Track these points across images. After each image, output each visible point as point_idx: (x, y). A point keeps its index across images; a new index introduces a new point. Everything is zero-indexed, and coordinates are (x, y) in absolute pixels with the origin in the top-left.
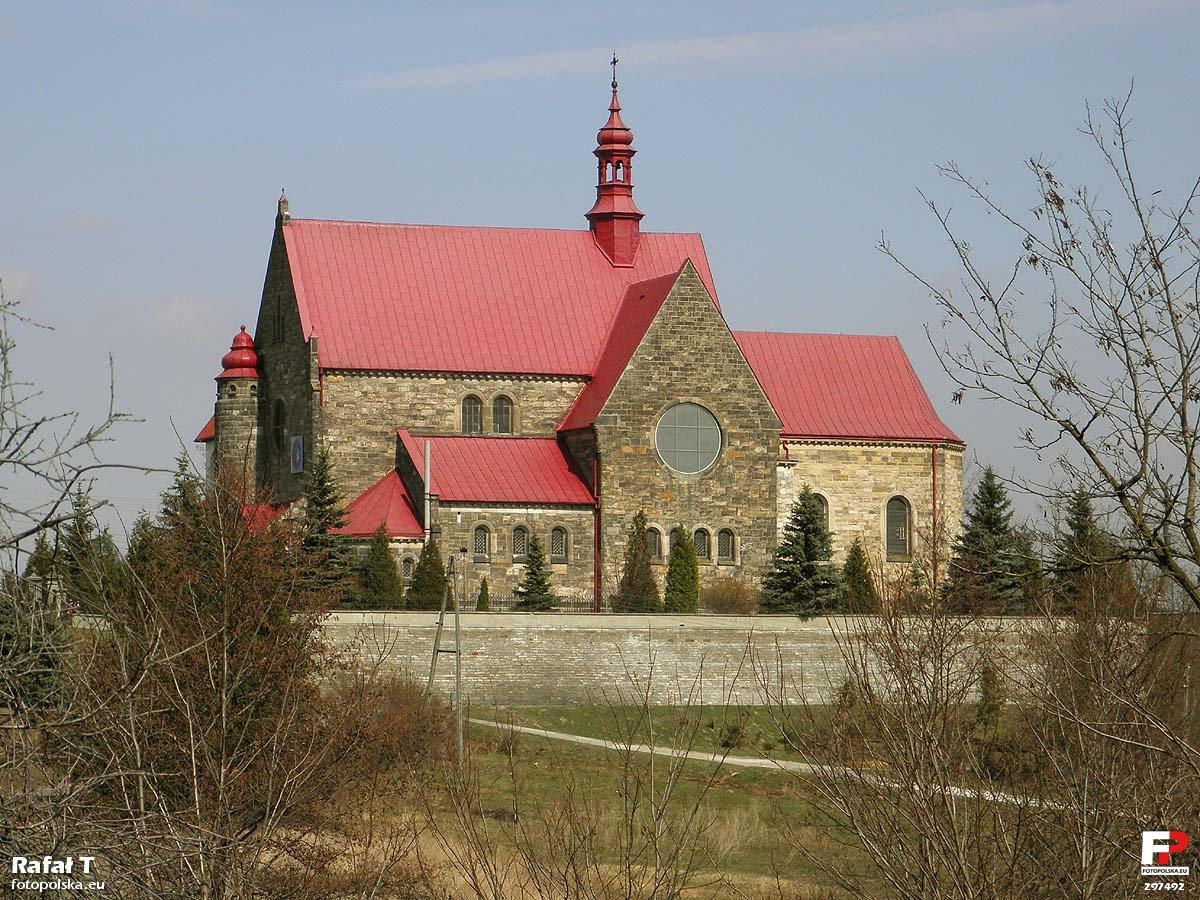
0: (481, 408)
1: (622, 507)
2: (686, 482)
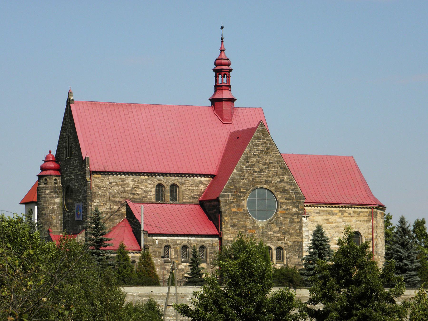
0: (164, 190)
1: (232, 236)
2: (261, 225)
